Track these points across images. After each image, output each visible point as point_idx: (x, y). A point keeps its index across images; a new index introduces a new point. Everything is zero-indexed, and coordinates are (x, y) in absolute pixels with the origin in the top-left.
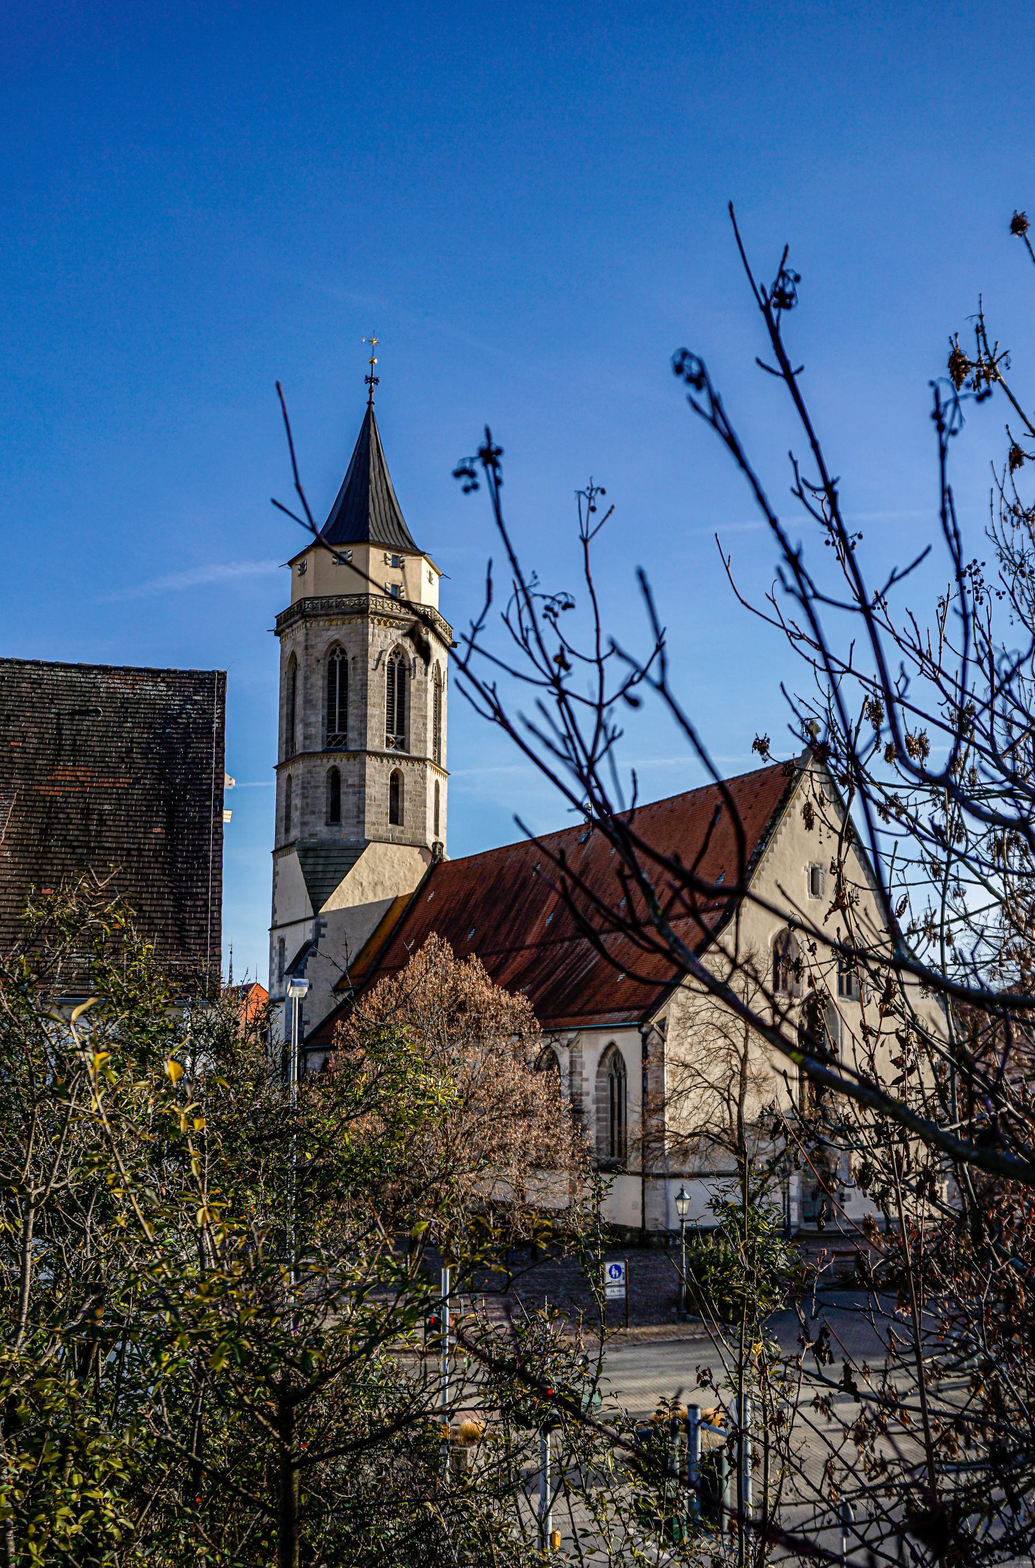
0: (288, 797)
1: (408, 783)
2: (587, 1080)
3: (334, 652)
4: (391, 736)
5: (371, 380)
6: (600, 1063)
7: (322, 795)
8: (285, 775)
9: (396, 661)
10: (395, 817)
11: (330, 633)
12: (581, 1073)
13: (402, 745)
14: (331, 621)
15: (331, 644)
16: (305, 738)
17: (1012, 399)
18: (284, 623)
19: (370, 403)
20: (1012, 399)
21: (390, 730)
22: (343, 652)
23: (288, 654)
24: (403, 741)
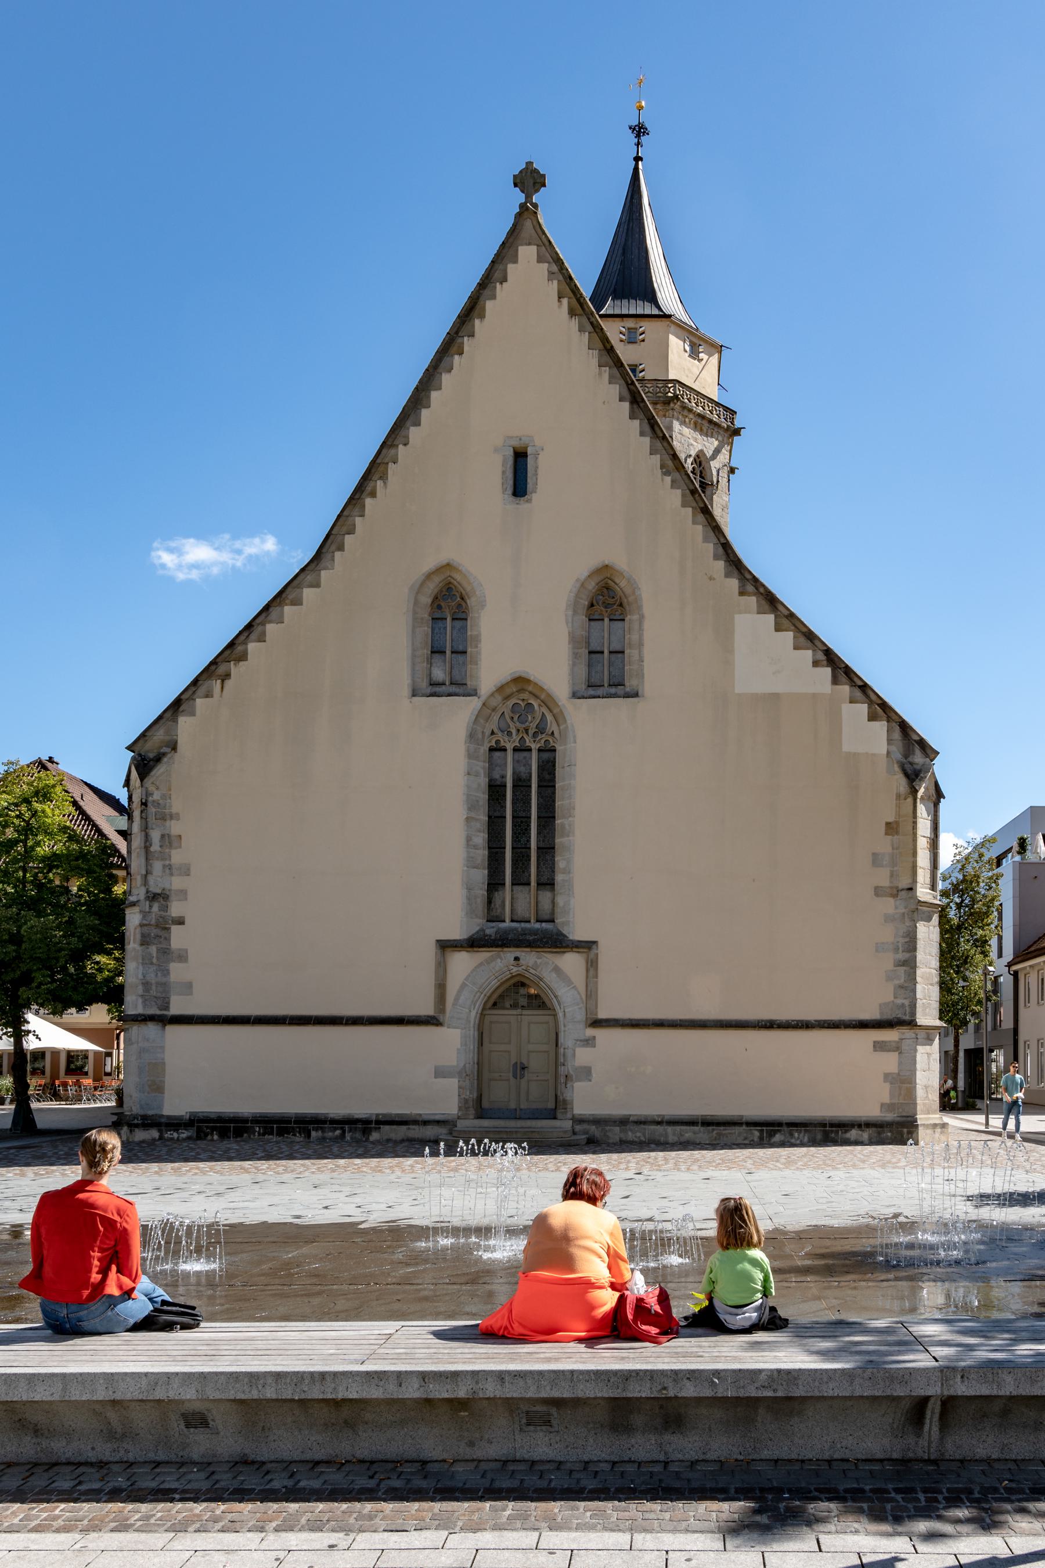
5: (640, 131)
17: (770, 1025)
20: (770, 1025)
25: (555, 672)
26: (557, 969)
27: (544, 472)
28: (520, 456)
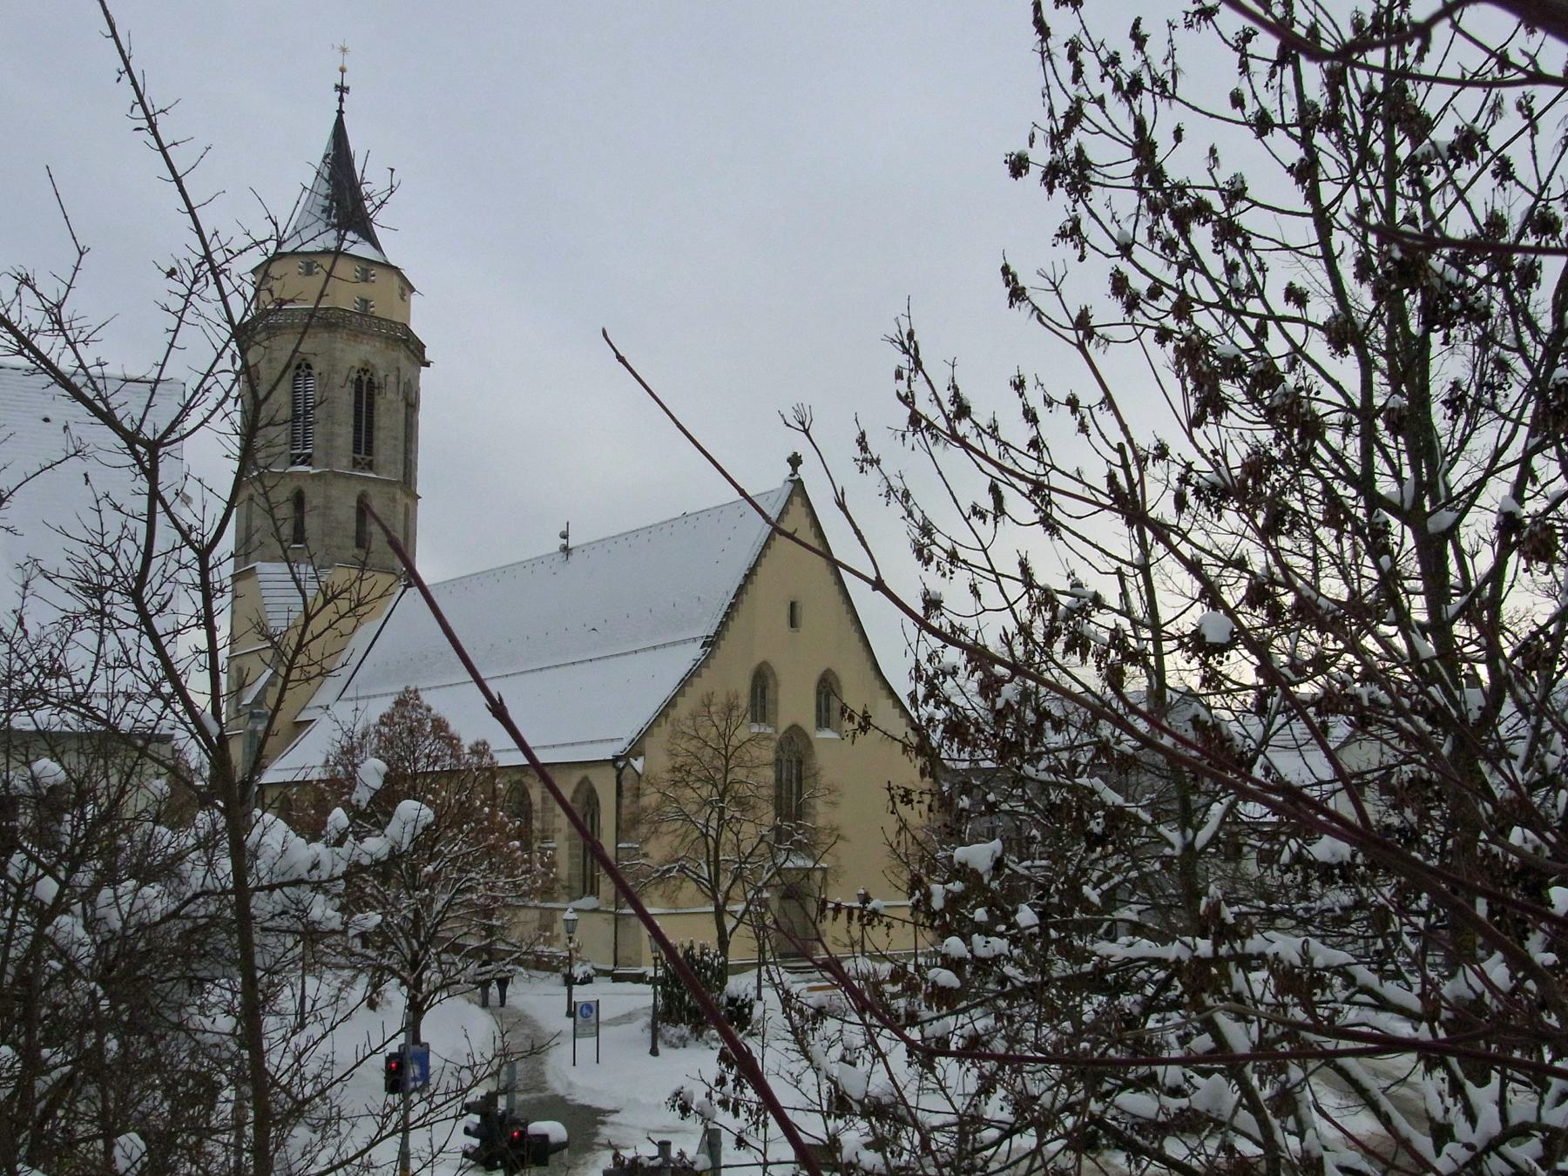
5: (342, 89)
7: (312, 524)
9: (365, 379)
19: (340, 112)
21: (357, 449)
22: (309, 366)
25: (808, 721)
27: (805, 615)
28: (793, 605)
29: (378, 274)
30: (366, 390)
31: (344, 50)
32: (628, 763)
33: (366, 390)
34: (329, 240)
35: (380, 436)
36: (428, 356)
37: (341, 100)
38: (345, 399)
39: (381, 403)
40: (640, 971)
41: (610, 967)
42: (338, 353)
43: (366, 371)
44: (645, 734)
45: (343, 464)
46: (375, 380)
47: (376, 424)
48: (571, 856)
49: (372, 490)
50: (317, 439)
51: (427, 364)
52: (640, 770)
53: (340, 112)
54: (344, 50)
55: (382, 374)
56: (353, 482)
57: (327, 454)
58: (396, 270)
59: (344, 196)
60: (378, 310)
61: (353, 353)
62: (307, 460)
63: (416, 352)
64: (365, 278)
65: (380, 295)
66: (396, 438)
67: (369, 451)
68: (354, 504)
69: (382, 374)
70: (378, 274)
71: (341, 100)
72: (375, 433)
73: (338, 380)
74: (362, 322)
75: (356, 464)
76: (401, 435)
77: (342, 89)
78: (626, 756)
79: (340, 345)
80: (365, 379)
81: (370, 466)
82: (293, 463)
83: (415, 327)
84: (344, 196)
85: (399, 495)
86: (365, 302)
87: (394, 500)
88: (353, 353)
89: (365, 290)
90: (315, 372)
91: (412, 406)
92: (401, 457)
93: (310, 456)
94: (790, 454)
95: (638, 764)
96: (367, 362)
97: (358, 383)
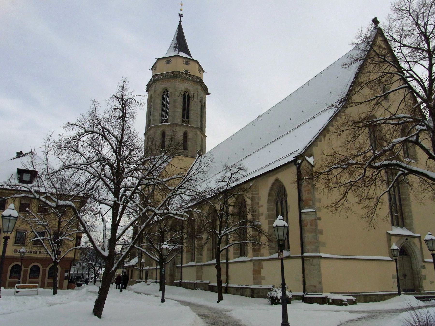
0: (148, 143)
1: (190, 135)
2: (262, 206)
3: (164, 92)
4: (184, 119)
5: (181, 15)
6: (269, 195)
8: (147, 136)
9: (187, 94)
10: (185, 148)
11: (163, 86)
12: (258, 203)
13: (188, 122)
14: (164, 81)
15: (163, 89)
16: (153, 121)
18: (149, 86)
19: (180, 22)
21: (183, 117)
22: (168, 91)
23: (150, 95)
24: (189, 121)
26: (414, 243)
29: (191, 62)
30: (187, 98)
31: (182, 5)
32: (304, 159)
33: (187, 98)
34: (175, 53)
35: (192, 113)
36: (209, 91)
37: (181, 18)
38: (180, 100)
39: (192, 102)
40: (324, 295)
41: (301, 293)
42: (177, 86)
43: (187, 92)
44: (313, 144)
45: (179, 120)
46: (190, 95)
47: (190, 109)
48: (269, 201)
49: (189, 130)
50: (170, 113)
51: (208, 94)
52: (312, 163)
53: (180, 22)
54: (182, 5)
55: (192, 93)
56: (182, 127)
57: (173, 118)
58: (197, 62)
59: (181, 42)
60: (191, 73)
61: (183, 86)
62: (167, 121)
63: (205, 89)
64: (187, 63)
65: (193, 70)
66: (197, 113)
67: (188, 117)
68: (183, 135)
69: (192, 93)
70: (191, 62)
71: (181, 18)
72: (190, 112)
73: (177, 94)
74: (185, 76)
75: (183, 121)
76: (199, 113)
77: (181, 15)
78: (301, 156)
79: (177, 83)
80: (187, 94)
81: (188, 122)
82: (162, 123)
83: (205, 80)
84: (181, 42)
85: (198, 133)
86: (187, 71)
87: (196, 134)
88: (183, 86)
89: (187, 68)
90: (169, 93)
91: (203, 106)
92: (199, 119)
93: (167, 119)
94: (373, 18)
95: (311, 160)
96: (187, 89)
97: (184, 96)
